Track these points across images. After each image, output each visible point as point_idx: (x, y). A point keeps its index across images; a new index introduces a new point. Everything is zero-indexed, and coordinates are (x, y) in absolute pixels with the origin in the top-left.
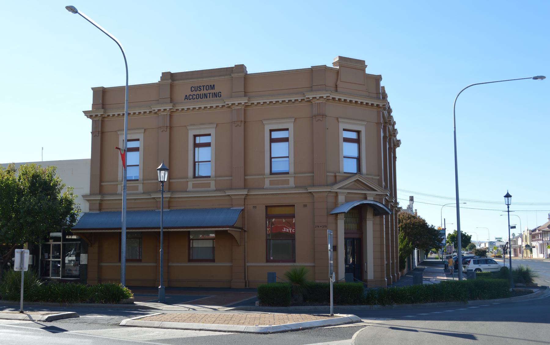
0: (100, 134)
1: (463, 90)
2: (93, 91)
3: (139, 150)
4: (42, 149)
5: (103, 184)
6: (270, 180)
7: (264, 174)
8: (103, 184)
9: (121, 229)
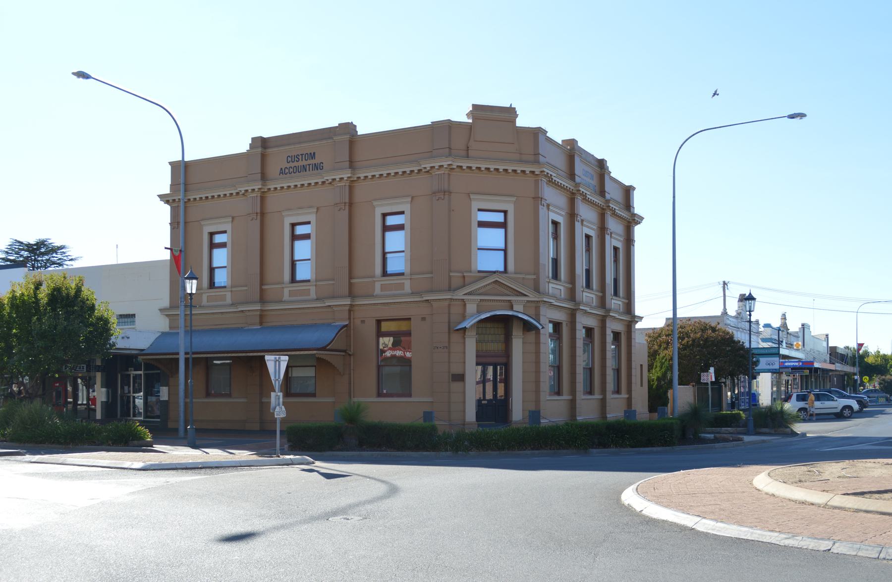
0: (259, 217)
1: (694, 135)
4: (117, 247)
7: (374, 277)
9: (178, 354)
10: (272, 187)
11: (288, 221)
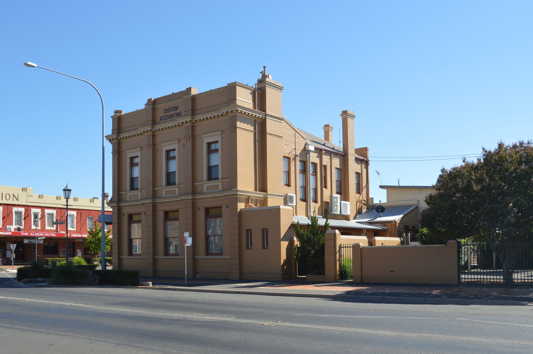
0: (152, 147)
2: (113, 119)
3: (218, 150)
5: (195, 184)
6: (207, 186)
7: (203, 181)
8: (195, 184)
10: (198, 119)
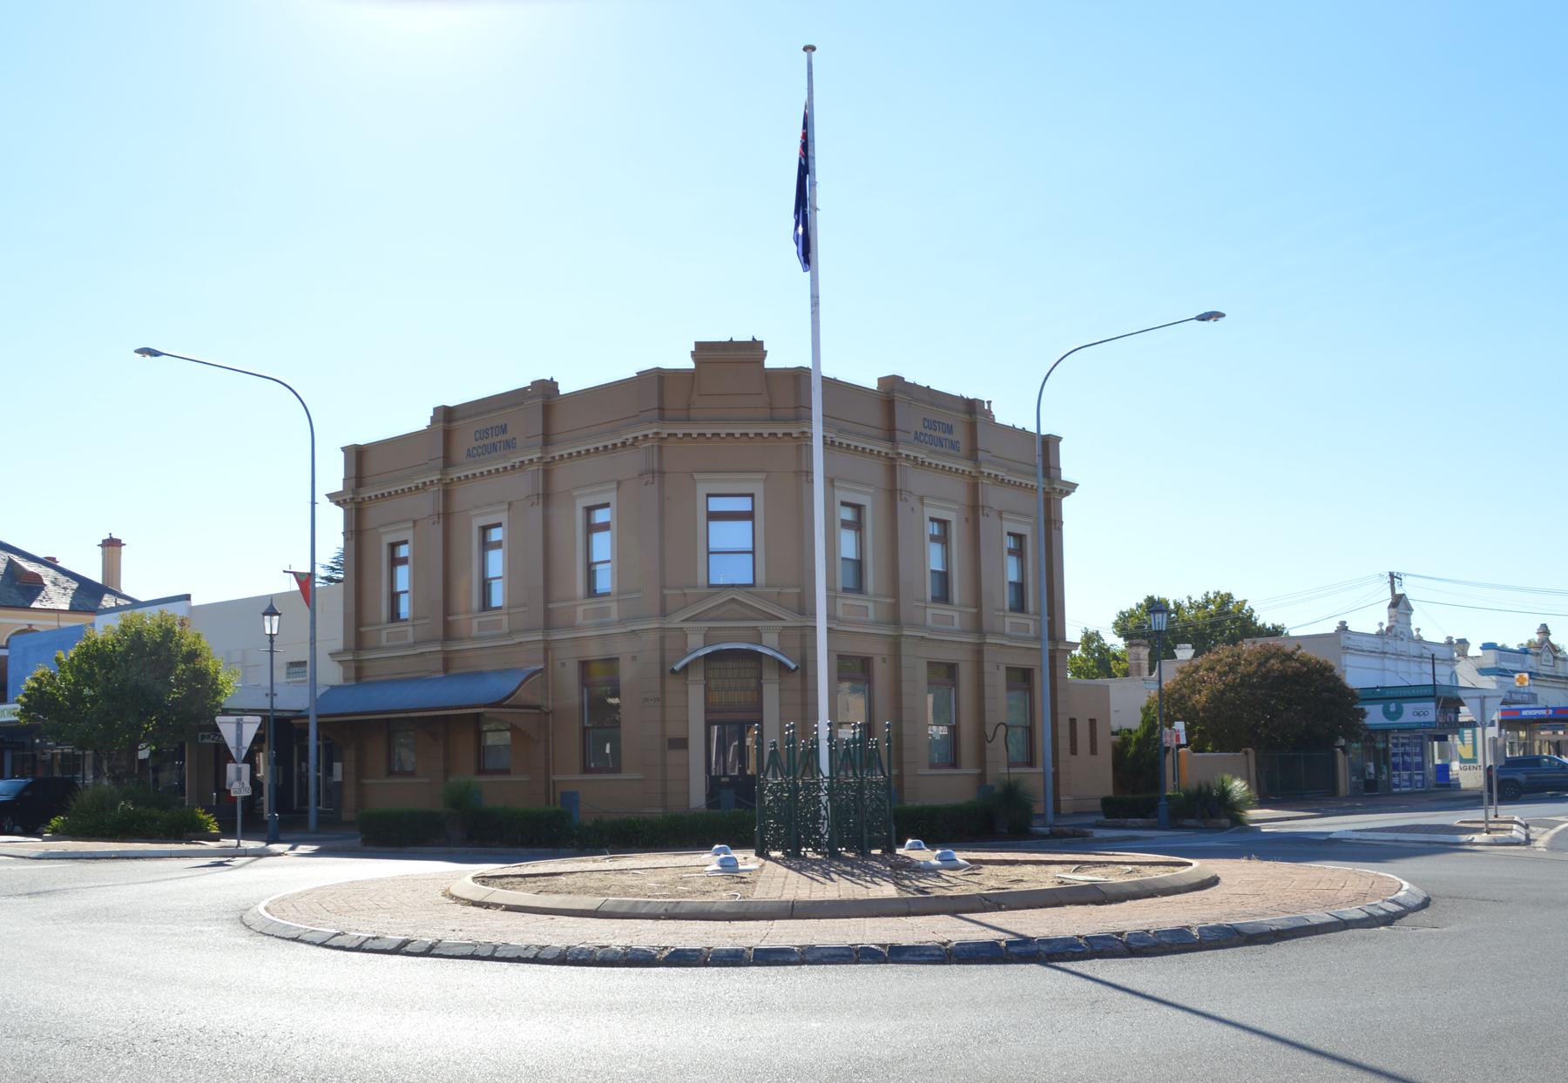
1: (1064, 357)
5: (363, 629)
8: (363, 629)
9: (307, 717)
11: (581, 503)
